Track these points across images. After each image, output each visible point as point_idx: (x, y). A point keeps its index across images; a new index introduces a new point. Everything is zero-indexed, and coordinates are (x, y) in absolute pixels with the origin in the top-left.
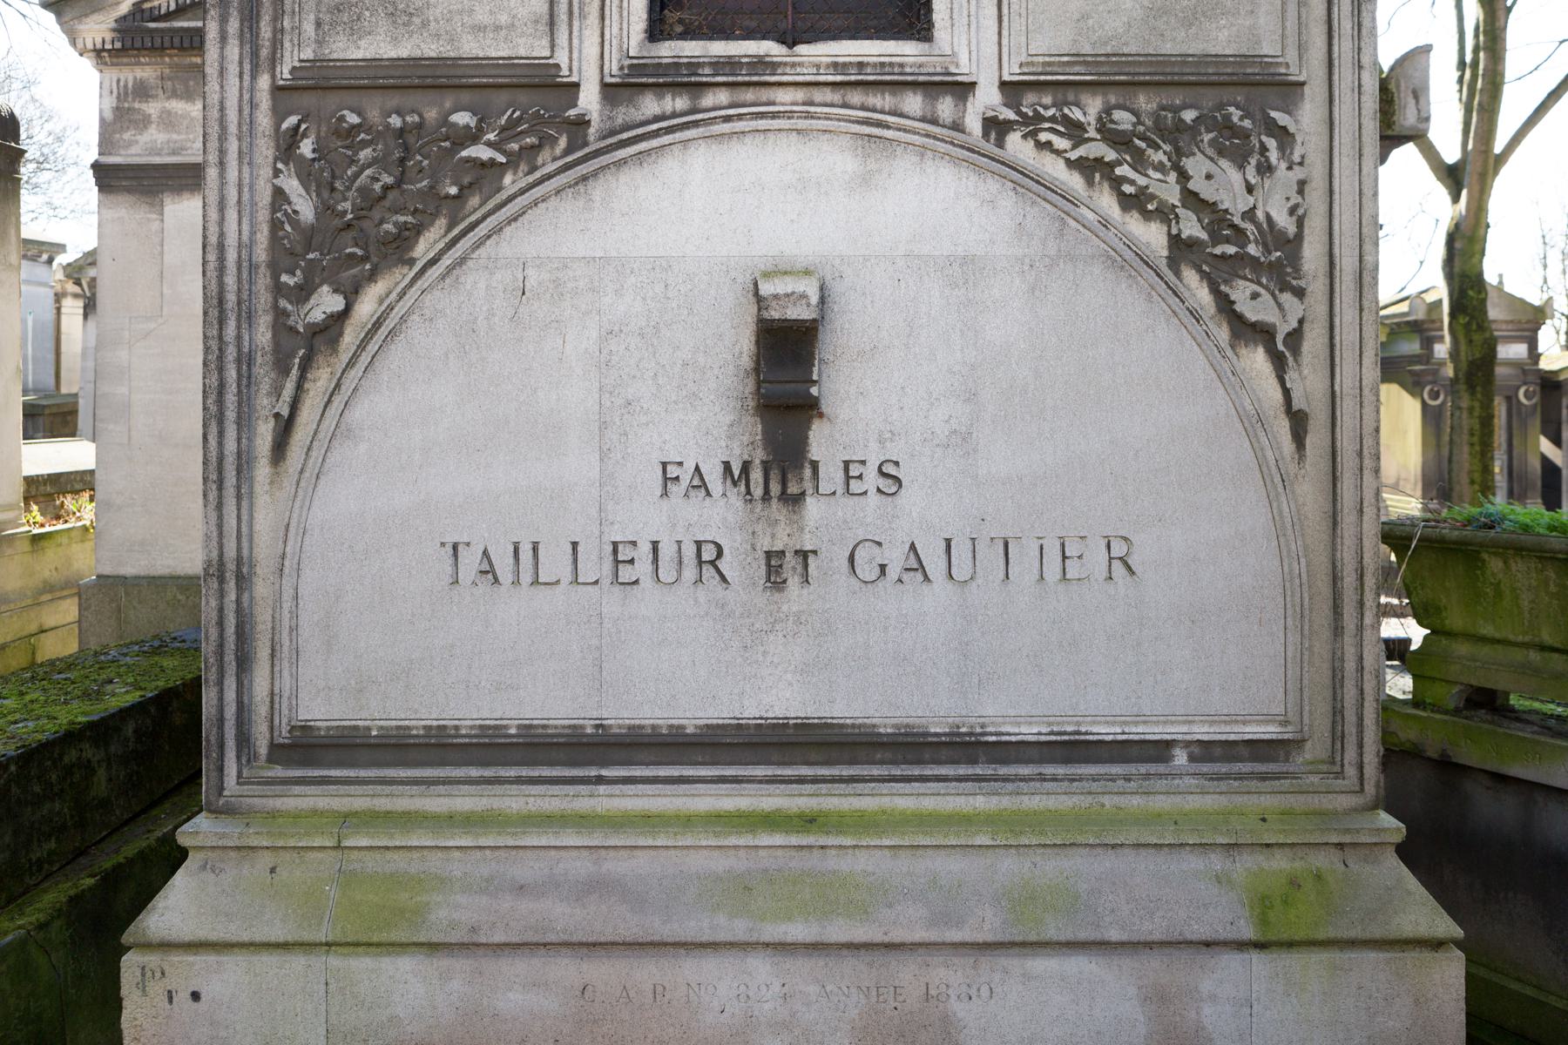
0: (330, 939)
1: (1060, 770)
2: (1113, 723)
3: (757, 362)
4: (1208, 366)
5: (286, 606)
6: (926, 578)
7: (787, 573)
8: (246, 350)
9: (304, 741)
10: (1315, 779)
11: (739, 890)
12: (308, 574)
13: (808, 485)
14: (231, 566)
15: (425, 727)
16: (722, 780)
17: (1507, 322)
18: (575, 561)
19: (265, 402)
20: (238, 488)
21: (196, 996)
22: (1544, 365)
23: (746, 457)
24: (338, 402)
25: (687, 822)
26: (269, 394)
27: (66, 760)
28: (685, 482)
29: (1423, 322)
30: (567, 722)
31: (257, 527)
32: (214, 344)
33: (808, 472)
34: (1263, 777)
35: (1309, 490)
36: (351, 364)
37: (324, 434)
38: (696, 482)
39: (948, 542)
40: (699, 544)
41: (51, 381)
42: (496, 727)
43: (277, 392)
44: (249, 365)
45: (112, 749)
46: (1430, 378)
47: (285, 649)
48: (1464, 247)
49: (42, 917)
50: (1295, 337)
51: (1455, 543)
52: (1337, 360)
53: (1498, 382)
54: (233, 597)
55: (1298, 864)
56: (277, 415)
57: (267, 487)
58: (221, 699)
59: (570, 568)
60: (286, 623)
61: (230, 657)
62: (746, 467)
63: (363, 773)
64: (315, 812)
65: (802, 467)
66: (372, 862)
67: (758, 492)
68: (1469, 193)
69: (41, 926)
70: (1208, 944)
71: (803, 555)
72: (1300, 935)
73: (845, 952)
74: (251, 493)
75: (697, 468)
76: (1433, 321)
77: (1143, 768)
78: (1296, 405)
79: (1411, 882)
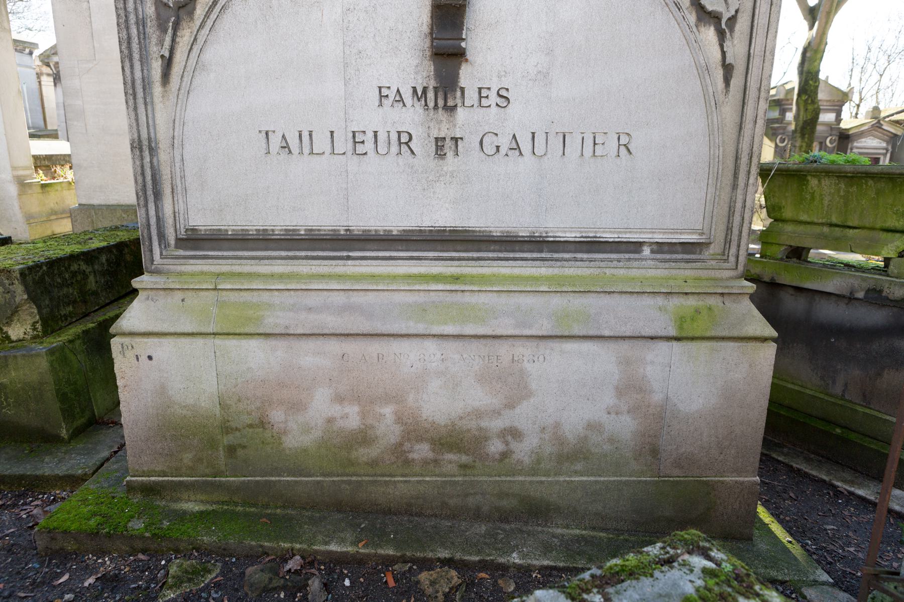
0: (215, 331)
1: (585, 256)
2: (614, 233)
3: (432, 29)
4: (682, 37)
5: (177, 165)
6: (521, 154)
7: (446, 149)
8: (141, 17)
9: (193, 237)
10: (713, 263)
11: (422, 310)
12: (187, 148)
13: (459, 101)
14: (145, 143)
15: (256, 230)
16: (412, 258)
17: (827, 101)
18: (333, 141)
19: (155, 49)
20: (145, 99)
21: (150, 358)
22: (843, 125)
23: (425, 85)
24: (196, 49)
25: (394, 278)
26: (157, 45)
27: (72, 268)
28: (391, 98)
29: (782, 100)
30: (330, 228)
31: (157, 122)
32: (122, 13)
33: (459, 93)
34: (688, 261)
35: (729, 111)
36: (201, 26)
37: (190, 68)
38: (398, 98)
39: (533, 134)
40: (399, 133)
41: (42, 123)
42: (294, 230)
43: (161, 43)
44: (144, 26)
45: (96, 267)
46: (781, 131)
47: (179, 188)
48: (811, 55)
49: (70, 338)
50: (733, 20)
51: (794, 171)
52: (754, 35)
53: (817, 134)
54: (148, 160)
55: (700, 303)
56: (162, 56)
57: (161, 99)
58: (147, 214)
59: (330, 146)
60: (178, 174)
61: (150, 192)
62: (425, 90)
63: (225, 253)
64: (202, 273)
65: (456, 90)
66: (233, 296)
67: (431, 104)
68: (819, 24)
69: (70, 341)
70: (652, 338)
71: (456, 140)
72: (698, 334)
73: (473, 340)
74: (152, 102)
75: (398, 91)
76: (788, 100)
77: (627, 256)
78: (728, 61)
79: (756, 312)
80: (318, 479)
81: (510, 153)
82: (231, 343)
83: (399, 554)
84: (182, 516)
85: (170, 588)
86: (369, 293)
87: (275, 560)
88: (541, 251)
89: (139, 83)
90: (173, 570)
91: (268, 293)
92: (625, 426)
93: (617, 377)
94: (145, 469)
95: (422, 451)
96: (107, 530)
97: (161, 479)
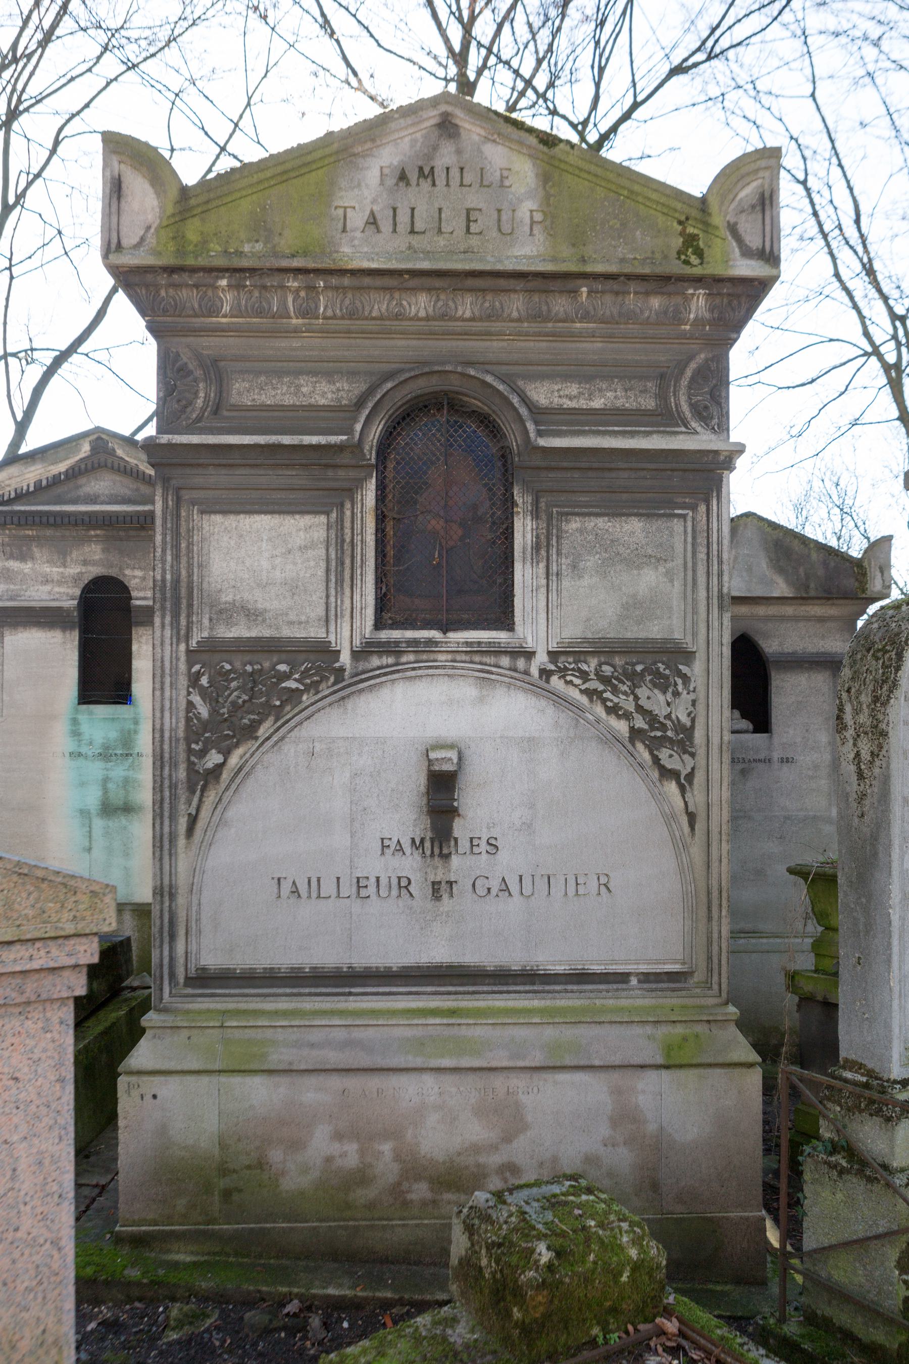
1: (575, 987)
5: (194, 909)
7: (442, 892)
10: (698, 990)
11: (420, 1045)
13: (453, 850)
14: (166, 889)
20: (170, 850)
24: (220, 808)
25: (393, 1013)
32: (158, 779)
33: (452, 843)
34: (673, 990)
35: (696, 851)
39: (521, 877)
40: (399, 878)
50: (690, 776)
55: (688, 1031)
58: (161, 954)
60: (194, 918)
61: (166, 934)
62: (422, 841)
63: (232, 991)
64: (209, 1011)
66: (238, 1034)
67: (428, 853)
71: (450, 883)
72: (685, 1062)
77: (615, 986)
80: (315, 1224)
81: (500, 894)
82: (236, 1080)
83: (397, 1297)
84: (176, 1265)
85: (173, 1329)
86: (370, 1028)
87: (272, 1305)
88: (534, 984)
89: (166, 836)
90: (174, 1313)
91: (272, 1030)
92: (623, 1159)
93: (610, 1107)
94: (136, 1218)
95: (420, 1191)
96: (104, 1277)
97: (151, 1228)
